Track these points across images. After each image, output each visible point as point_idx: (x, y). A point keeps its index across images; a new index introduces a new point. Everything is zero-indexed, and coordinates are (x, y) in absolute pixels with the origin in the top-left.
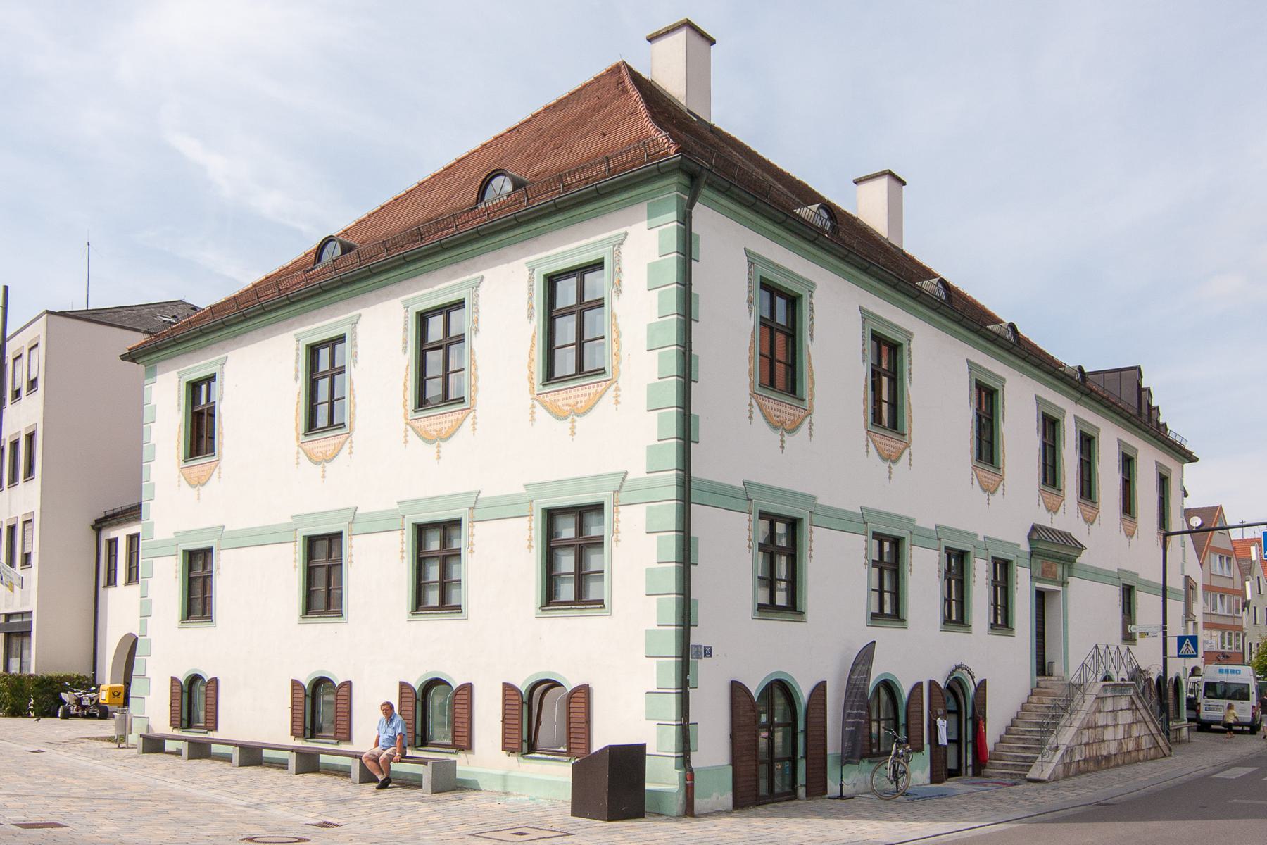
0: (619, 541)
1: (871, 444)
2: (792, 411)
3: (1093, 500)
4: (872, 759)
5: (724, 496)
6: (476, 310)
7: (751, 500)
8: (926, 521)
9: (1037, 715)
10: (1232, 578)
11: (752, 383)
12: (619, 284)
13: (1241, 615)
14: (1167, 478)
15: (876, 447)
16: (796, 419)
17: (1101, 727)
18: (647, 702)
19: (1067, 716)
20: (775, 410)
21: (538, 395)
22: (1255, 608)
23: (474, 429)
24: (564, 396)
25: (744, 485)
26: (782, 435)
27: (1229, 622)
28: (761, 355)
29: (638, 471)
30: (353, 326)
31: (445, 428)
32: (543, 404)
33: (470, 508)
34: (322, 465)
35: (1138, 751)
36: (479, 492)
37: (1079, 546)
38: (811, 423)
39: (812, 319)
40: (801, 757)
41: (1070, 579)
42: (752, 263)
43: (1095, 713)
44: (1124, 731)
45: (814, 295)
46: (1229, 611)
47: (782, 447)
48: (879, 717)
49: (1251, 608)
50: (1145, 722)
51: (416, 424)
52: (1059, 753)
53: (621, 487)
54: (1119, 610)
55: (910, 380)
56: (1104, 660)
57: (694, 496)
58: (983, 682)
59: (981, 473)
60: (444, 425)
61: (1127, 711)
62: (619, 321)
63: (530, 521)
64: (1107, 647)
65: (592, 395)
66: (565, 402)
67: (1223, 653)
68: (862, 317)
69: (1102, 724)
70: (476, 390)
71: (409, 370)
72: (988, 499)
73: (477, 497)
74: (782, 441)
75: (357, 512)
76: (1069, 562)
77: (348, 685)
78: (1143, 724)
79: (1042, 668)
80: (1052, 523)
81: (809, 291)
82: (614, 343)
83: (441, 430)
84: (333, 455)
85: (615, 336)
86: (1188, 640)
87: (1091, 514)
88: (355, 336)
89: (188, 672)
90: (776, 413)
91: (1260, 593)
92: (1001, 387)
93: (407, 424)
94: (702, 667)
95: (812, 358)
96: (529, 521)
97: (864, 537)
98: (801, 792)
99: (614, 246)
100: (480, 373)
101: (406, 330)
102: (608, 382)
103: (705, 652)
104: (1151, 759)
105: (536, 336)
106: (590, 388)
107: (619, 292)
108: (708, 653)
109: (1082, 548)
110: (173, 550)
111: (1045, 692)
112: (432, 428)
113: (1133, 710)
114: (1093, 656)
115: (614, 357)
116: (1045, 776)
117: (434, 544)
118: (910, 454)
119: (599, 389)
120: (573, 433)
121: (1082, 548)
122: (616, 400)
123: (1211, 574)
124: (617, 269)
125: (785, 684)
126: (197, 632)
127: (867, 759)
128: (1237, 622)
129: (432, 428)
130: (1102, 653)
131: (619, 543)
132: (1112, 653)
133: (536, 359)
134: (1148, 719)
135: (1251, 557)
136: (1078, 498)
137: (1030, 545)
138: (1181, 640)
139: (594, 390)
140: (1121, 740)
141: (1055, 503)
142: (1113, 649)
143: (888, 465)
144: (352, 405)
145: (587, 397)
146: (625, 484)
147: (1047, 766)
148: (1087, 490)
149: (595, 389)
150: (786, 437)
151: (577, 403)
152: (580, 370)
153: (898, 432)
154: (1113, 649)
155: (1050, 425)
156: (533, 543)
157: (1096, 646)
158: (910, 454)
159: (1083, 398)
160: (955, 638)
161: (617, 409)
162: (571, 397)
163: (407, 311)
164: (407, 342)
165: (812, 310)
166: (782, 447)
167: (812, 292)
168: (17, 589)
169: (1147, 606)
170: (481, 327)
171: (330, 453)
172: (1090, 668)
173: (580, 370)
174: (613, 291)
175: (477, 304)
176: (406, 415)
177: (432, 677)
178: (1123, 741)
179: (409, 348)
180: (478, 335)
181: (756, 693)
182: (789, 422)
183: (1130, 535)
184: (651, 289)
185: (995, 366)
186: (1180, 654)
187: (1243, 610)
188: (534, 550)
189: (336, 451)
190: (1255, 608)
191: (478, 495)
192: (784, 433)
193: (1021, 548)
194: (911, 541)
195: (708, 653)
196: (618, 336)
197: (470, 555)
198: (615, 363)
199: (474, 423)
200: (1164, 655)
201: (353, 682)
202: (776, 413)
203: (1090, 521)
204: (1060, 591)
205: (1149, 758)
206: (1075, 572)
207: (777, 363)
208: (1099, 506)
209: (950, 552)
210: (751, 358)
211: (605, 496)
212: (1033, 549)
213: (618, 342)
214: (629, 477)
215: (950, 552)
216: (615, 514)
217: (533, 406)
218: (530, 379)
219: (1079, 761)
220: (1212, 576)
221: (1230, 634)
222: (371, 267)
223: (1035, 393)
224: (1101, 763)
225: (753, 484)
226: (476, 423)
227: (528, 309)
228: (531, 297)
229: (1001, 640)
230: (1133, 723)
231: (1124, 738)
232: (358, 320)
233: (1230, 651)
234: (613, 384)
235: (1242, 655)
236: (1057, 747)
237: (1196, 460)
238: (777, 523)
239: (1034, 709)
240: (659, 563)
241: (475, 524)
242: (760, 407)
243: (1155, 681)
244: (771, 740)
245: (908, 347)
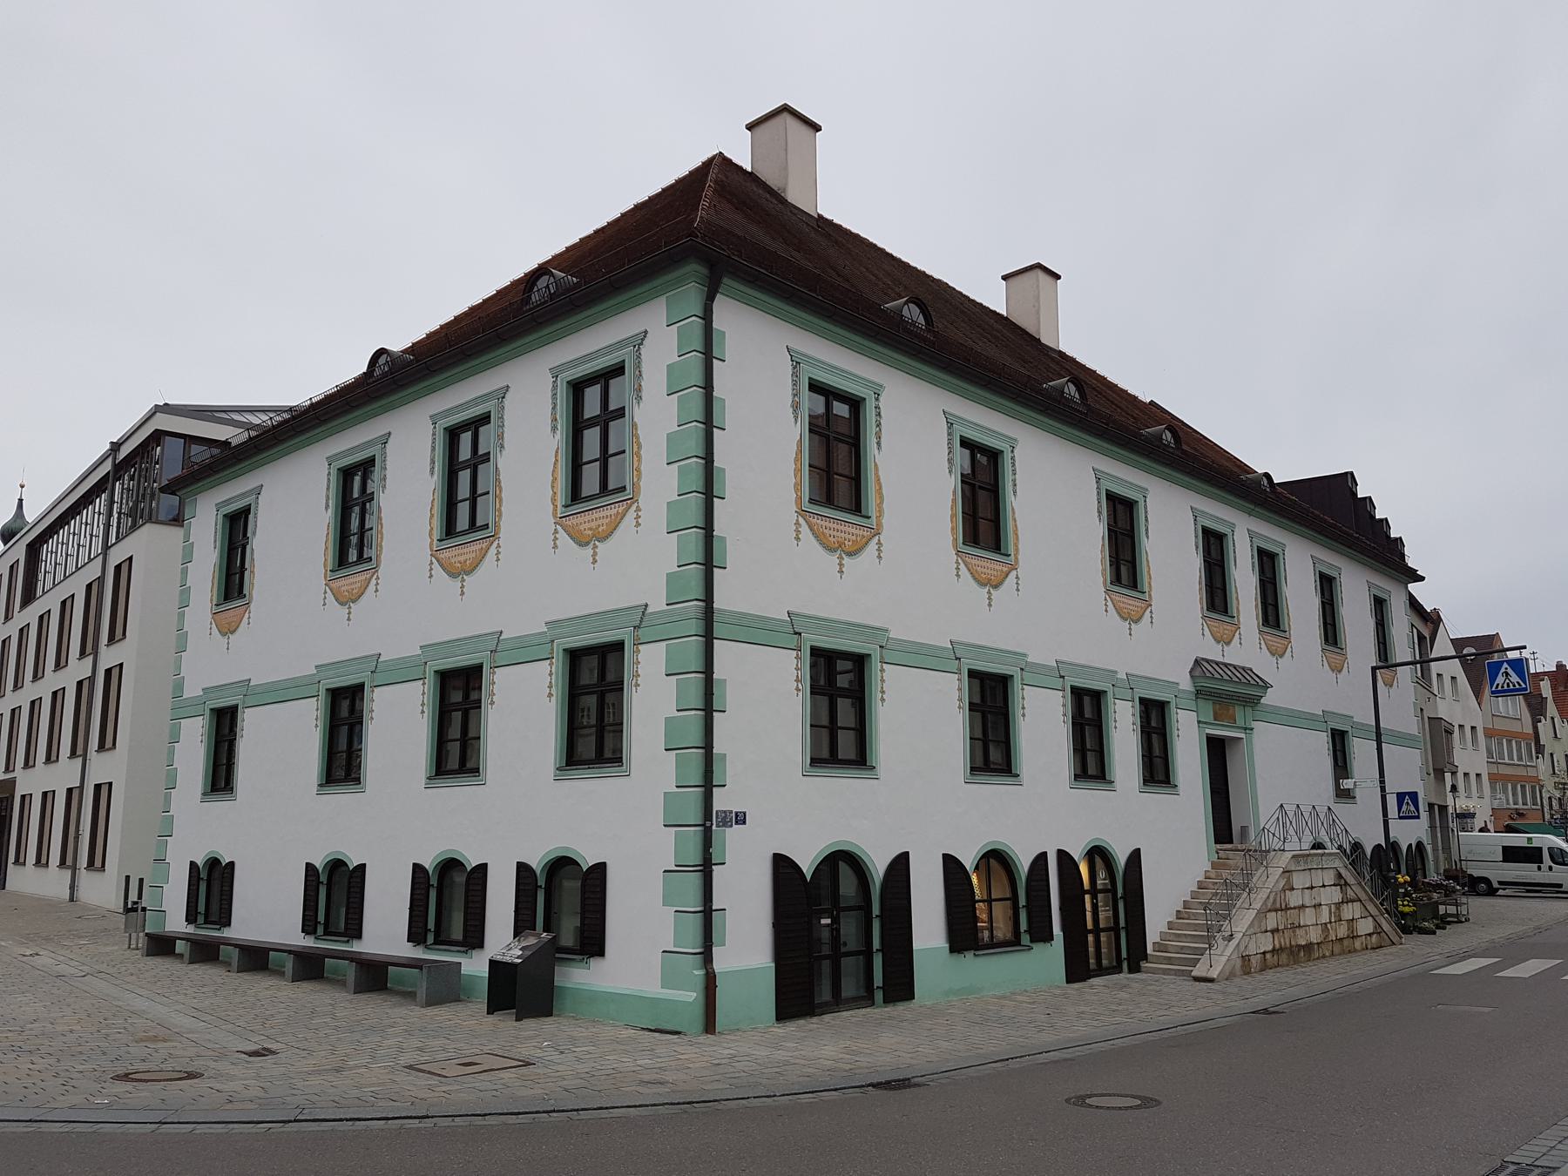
0: (639, 685)
1: (962, 566)
2: (854, 531)
4: (977, 953)
5: (757, 632)
7: (800, 634)
10: (1520, 720)
11: (799, 500)
13: (1534, 764)
15: (969, 570)
16: (859, 539)
17: (1295, 908)
19: (1245, 894)
20: (830, 529)
21: (561, 518)
22: (1552, 755)
25: (789, 617)
26: (841, 558)
27: (1521, 772)
28: (810, 466)
29: (658, 604)
33: (492, 651)
34: (347, 606)
35: (1352, 938)
37: (1261, 683)
38: (879, 543)
39: (879, 425)
40: (877, 950)
42: (797, 362)
43: (1284, 890)
44: (1330, 913)
45: (881, 398)
46: (1520, 759)
47: (841, 572)
48: (990, 896)
49: (1547, 756)
50: (1361, 901)
51: (443, 555)
52: (1234, 943)
54: (1328, 763)
55: (1015, 492)
56: (1309, 824)
58: (1135, 856)
59: (1116, 597)
61: (1333, 887)
64: (1298, 806)
66: (587, 526)
67: (1516, 809)
68: (948, 422)
69: (1296, 905)
71: (436, 494)
72: (1130, 629)
74: (841, 565)
75: (380, 660)
76: (1252, 702)
77: (231, 865)
78: (1359, 903)
79: (1223, 829)
80: (1223, 655)
81: (875, 393)
83: (465, 562)
85: (635, 449)
86: (1407, 797)
87: (1279, 645)
90: (831, 532)
91: (1556, 736)
92: (1143, 499)
94: (731, 840)
95: (880, 468)
97: (957, 675)
98: (879, 996)
101: (433, 449)
102: (629, 502)
103: (736, 818)
104: (1373, 948)
107: (639, 398)
108: (741, 819)
109: (1266, 686)
110: (200, 709)
111: (1225, 864)
112: (456, 559)
113: (1341, 886)
114: (1278, 818)
116: (1214, 974)
117: (456, 697)
118: (1017, 578)
119: (620, 510)
123: (1493, 715)
124: (637, 372)
125: (1102, 850)
126: (457, 794)
127: (973, 952)
128: (1532, 772)
129: (456, 559)
130: (1291, 814)
132: (1306, 815)
134: (1363, 896)
135: (1541, 694)
138: (1401, 797)
140: (1326, 924)
141: (1226, 632)
142: (1322, 811)
143: (987, 590)
144: (379, 536)
147: (1218, 961)
148: (1272, 613)
150: (846, 560)
151: (599, 525)
152: (604, 489)
154: (1322, 811)
155: (1214, 545)
156: (554, 691)
157: (1282, 806)
158: (1017, 578)
159: (1257, 509)
160: (1091, 796)
163: (435, 427)
165: (879, 414)
166: (841, 572)
167: (879, 395)
169: (1362, 751)
172: (1274, 835)
173: (604, 489)
175: (502, 417)
176: (431, 544)
178: (1329, 925)
180: (504, 452)
181: (970, 868)
182: (850, 543)
183: (1337, 669)
185: (1129, 477)
186: (1401, 815)
187: (1537, 758)
189: (362, 589)
190: (1552, 755)
191: (500, 635)
192: (844, 556)
193: (1180, 687)
194: (1022, 679)
195: (741, 819)
197: (490, 706)
199: (498, 553)
200: (1384, 816)
201: (236, 862)
202: (831, 532)
203: (1278, 653)
205: (1369, 947)
207: (835, 476)
209: (1078, 694)
210: (798, 471)
212: (1198, 688)
214: (650, 610)
215: (1078, 694)
217: (556, 532)
218: (554, 500)
219: (1264, 953)
220: (1494, 718)
221: (1523, 787)
222: (396, 378)
224: (1294, 954)
225: (798, 615)
229: (1157, 799)
230: (1342, 902)
231: (1331, 922)
233: (1525, 807)
235: (1540, 812)
236: (1232, 935)
237: (1423, 579)
238: (838, 661)
240: (678, 711)
242: (809, 526)
243: (1369, 852)
244: (835, 929)
245: (1010, 455)
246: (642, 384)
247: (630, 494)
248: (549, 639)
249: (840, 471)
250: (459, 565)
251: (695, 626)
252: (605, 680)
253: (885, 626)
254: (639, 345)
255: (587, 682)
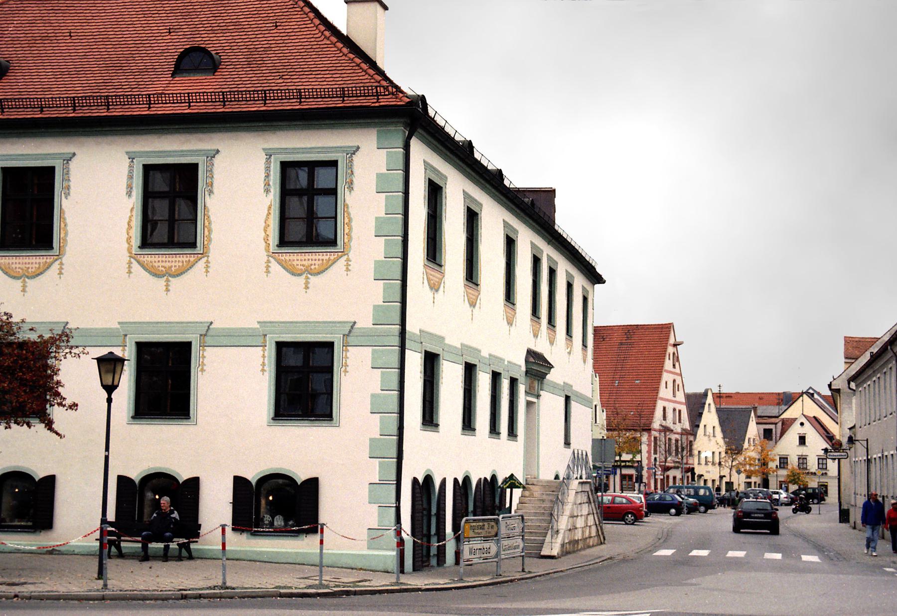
0: (347, 372)
3: (511, 301)
6: (210, 176)
8: (454, 341)
9: (533, 507)
12: (352, 183)
14: (514, 241)
18: (370, 491)
21: (273, 253)
23: (207, 272)
24: (299, 257)
29: (365, 321)
30: (65, 162)
31: (175, 266)
32: (279, 263)
33: (201, 335)
34: (21, 280)
36: (211, 323)
41: (542, 393)
53: (350, 332)
57: (408, 344)
59: (429, 271)
60: (173, 264)
62: (350, 210)
63: (264, 351)
65: (325, 261)
70: (210, 240)
73: (209, 327)
82: (346, 226)
84: (37, 273)
88: (68, 171)
89: (32, 471)
93: (130, 257)
96: (262, 350)
99: (347, 154)
100: (213, 226)
105: (273, 207)
106: (323, 255)
107: (351, 188)
109: (550, 367)
115: (346, 236)
116: (555, 552)
119: (332, 258)
120: (307, 288)
121: (550, 367)
122: (347, 268)
124: (349, 171)
131: (347, 374)
133: (272, 226)
136: (424, 260)
137: (526, 366)
139: (327, 258)
145: (321, 262)
146: (353, 331)
149: (328, 256)
151: (311, 265)
153: (473, 281)
161: (347, 275)
162: (305, 260)
163: (132, 161)
164: (131, 188)
168: (712, 438)
170: (215, 190)
171: (33, 270)
174: (346, 187)
175: (211, 170)
177: (141, 477)
179: (134, 193)
184: (379, 192)
188: (266, 374)
196: (349, 221)
198: (346, 240)
204: (535, 403)
206: (545, 387)
208: (444, 271)
211: (336, 337)
213: (349, 224)
214: (356, 326)
216: (344, 352)
217: (268, 261)
218: (266, 240)
223: (424, 158)
226: (209, 267)
227: (265, 185)
228: (268, 176)
232: (71, 158)
234: (344, 255)
239: (528, 502)
241: (205, 348)
246: (354, 180)
247: (341, 249)
248: (261, 333)
249: (111, 380)
250: (163, 269)
251: (396, 341)
252: (401, 549)
253: (479, 348)
254: (352, 154)
255: (292, 187)
